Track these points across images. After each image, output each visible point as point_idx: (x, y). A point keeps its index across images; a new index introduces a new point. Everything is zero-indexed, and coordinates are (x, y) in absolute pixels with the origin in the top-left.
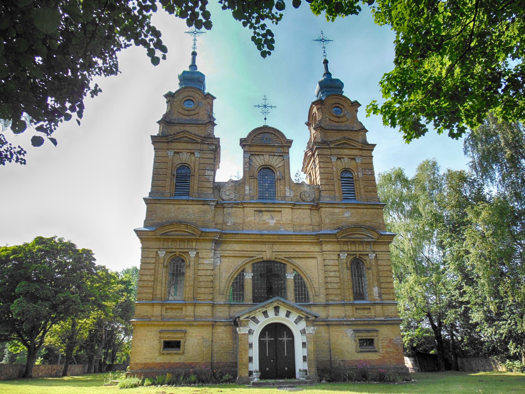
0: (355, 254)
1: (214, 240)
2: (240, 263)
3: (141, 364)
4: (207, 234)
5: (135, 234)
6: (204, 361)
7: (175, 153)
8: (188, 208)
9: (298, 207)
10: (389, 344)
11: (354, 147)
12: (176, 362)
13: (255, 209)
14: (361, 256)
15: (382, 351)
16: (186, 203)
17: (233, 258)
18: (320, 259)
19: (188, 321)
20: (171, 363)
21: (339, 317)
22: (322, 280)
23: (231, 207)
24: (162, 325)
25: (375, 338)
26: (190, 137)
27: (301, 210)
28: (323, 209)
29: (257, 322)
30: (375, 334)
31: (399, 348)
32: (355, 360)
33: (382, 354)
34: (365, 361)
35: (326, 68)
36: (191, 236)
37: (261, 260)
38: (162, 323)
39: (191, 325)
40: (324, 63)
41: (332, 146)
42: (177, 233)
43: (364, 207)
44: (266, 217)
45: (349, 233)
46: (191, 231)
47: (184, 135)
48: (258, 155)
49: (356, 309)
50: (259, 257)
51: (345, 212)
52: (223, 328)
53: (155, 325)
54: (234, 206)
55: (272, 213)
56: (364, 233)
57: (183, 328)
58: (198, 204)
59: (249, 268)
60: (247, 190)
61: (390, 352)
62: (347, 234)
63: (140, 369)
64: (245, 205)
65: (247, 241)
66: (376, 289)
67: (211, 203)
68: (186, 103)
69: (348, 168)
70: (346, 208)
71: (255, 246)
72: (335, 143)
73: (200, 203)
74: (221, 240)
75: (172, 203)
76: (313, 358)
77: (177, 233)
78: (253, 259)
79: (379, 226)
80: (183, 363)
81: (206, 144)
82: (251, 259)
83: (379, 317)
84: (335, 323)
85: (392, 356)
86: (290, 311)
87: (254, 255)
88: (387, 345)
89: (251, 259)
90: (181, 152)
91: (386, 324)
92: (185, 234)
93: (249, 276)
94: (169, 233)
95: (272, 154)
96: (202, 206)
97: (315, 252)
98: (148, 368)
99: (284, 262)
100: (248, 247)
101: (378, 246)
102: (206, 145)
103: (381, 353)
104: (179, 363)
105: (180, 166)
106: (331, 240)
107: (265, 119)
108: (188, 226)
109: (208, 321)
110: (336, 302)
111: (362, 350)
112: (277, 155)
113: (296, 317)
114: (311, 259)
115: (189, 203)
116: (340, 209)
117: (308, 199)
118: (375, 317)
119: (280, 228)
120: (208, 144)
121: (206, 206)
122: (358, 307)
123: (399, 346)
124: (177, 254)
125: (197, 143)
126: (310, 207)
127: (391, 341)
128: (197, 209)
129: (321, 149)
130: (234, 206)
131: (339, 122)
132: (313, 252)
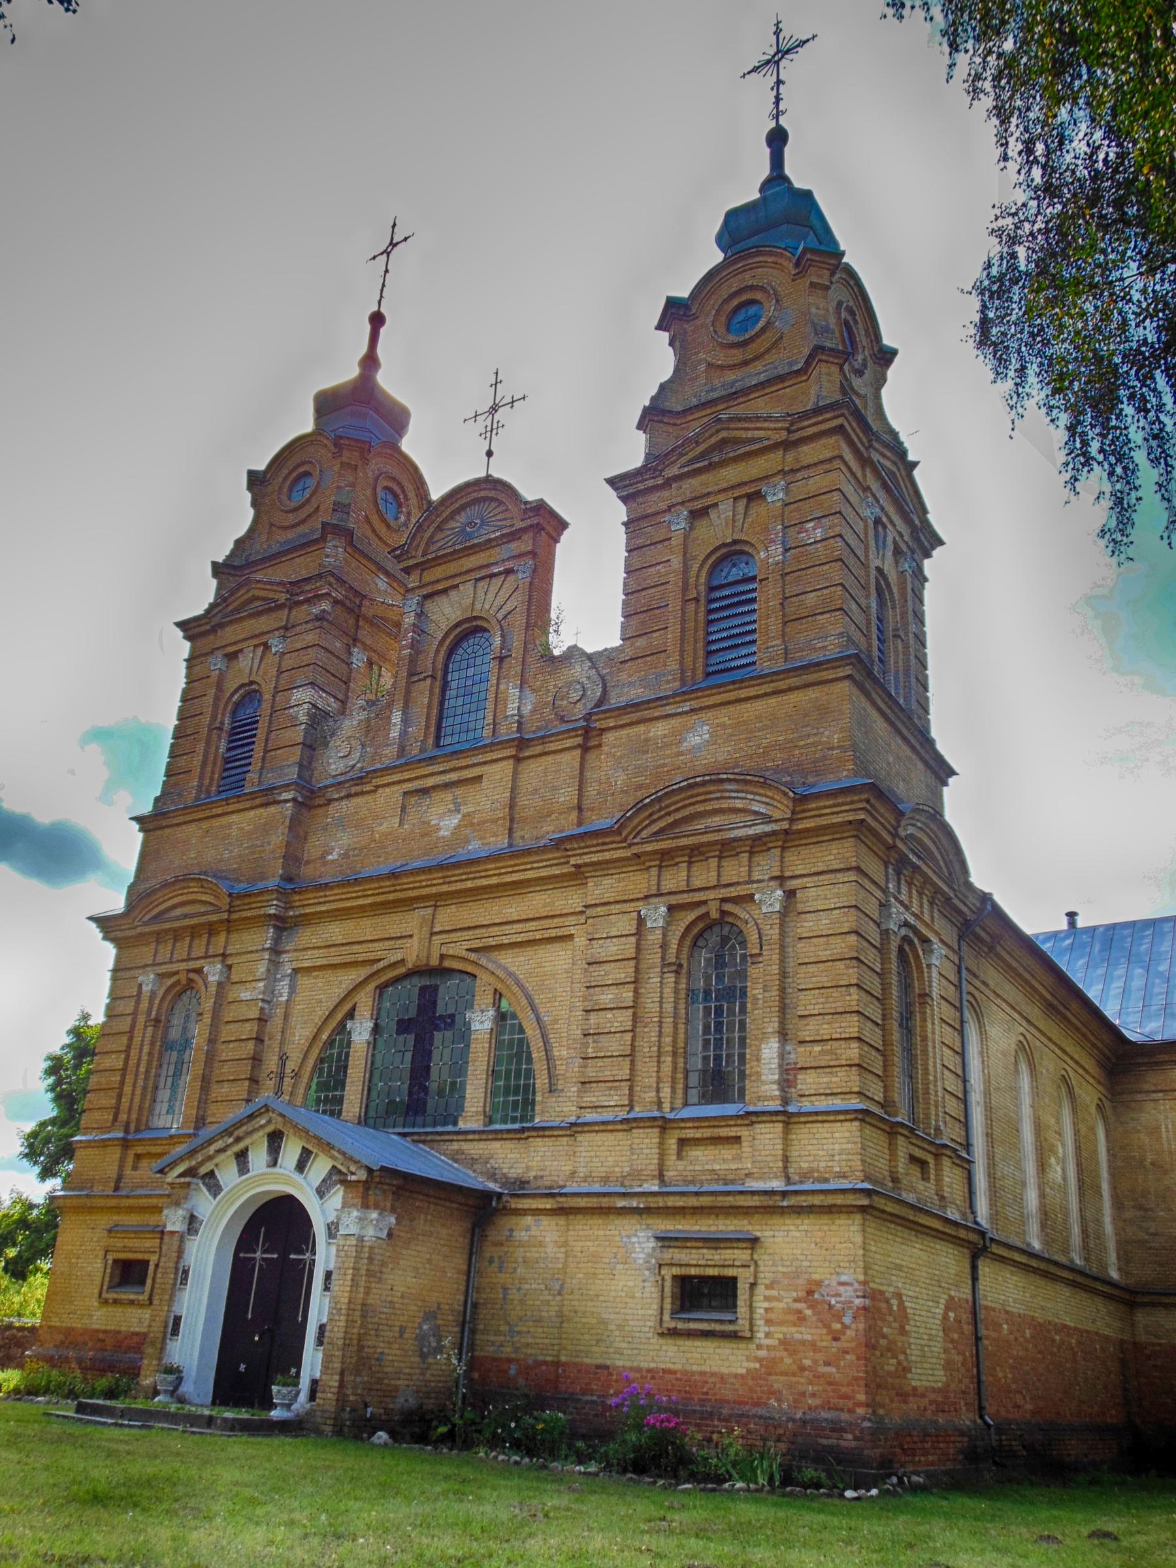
0: (705, 902)
4: (247, 900)
5: (95, 931)
7: (227, 656)
8: (230, 825)
9: (538, 749)
11: (757, 446)
12: (132, 1329)
13: (408, 786)
14: (728, 907)
15: (767, 1335)
20: (119, 1332)
21: (605, 1180)
24: (117, 1209)
25: (744, 1277)
27: (550, 758)
28: (609, 737)
29: (215, 1189)
30: (742, 1255)
31: (845, 1327)
32: (649, 1371)
33: (762, 1353)
34: (687, 1378)
35: (777, 161)
38: (113, 1202)
45: (678, 816)
50: (393, 959)
53: (101, 1209)
55: (458, 791)
56: (739, 804)
58: (252, 808)
59: (365, 1002)
60: (395, 725)
61: (803, 1343)
62: (670, 819)
69: (735, 542)
71: (386, 919)
72: (682, 455)
73: (258, 801)
74: (291, 913)
76: (341, 1335)
78: (376, 967)
79: (824, 758)
82: (368, 970)
83: (762, 1177)
85: (807, 1362)
86: (310, 1148)
87: (372, 956)
88: (789, 1311)
89: (368, 970)
91: (798, 1211)
92: (203, 909)
95: (483, 573)
96: (261, 810)
97: (566, 915)
100: (366, 928)
101: (804, 851)
103: (759, 1347)
105: (243, 697)
106: (607, 856)
107: (489, 454)
110: (607, 1116)
111: (680, 1325)
112: (500, 574)
113: (233, 1167)
114: (556, 946)
116: (674, 722)
120: (307, 601)
121: (273, 809)
122: (690, 1134)
123: (847, 1320)
127: (810, 1293)
129: (640, 500)
132: (561, 915)
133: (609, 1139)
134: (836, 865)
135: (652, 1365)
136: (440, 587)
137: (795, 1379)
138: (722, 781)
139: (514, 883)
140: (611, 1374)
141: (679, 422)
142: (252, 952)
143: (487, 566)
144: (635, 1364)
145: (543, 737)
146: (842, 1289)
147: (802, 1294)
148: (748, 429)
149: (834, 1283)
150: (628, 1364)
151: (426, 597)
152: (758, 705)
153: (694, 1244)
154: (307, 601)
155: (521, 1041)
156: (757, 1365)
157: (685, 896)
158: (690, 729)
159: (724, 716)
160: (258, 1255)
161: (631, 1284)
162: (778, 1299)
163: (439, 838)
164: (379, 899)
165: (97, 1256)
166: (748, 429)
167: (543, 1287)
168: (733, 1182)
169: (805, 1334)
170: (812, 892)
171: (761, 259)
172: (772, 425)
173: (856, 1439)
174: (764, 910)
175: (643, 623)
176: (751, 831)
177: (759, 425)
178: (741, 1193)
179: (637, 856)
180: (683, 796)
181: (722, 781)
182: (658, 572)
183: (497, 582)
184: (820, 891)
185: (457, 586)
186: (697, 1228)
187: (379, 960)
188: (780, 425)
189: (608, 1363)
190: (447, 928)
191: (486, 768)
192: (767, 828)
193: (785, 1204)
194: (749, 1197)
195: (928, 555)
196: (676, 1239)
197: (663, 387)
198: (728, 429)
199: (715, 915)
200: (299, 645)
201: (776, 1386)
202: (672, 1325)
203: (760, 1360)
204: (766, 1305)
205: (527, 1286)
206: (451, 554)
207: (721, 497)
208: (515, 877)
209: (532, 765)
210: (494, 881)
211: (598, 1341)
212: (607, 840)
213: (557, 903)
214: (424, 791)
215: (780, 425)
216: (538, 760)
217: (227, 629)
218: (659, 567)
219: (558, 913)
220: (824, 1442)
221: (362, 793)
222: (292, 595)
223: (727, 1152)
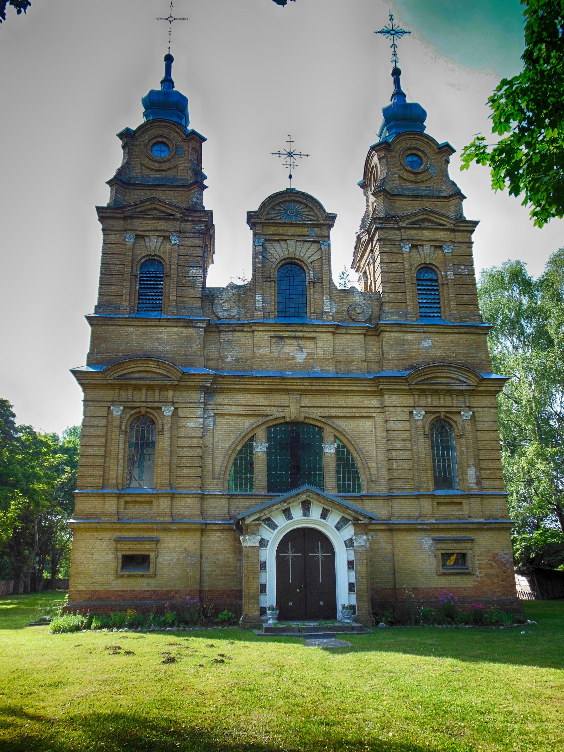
0: (439, 412)
1: (204, 387)
2: (247, 425)
3: (86, 592)
4: (192, 377)
8: (160, 333)
9: (344, 331)
10: (491, 562)
11: (441, 227)
12: (143, 589)
13: (272, 334)
15: (480, 573)
19: (161, 523)
20: (135, 591)
22: (382, 456)
23: (232, 331)
24: (120, 530)
25: (469, 552)
26: (162, 208)
27: (349, 336)
28: (387, 335)
30: (469, 545)
31: (507, 568)
32: (435, 588)
33: (479, 579)
37: (282, 421)
38: (118, 526)
40: (393, 75)
41: (404, 224)
43: (455, 331)
44: (290, 348)
45: (429, 376)
46: (165, 373)
48: (278, 241)
50: (278, 416)
51: (422, 340)
52: (219, 534)
53: (106, 530)
56: (454, 376)
57: (154, 535)
58: (176, 327)
59: (261, 434)
60: (258, 301)
61: (493, 575)
62: (426, 377)
63: (84, 600)
64: (253, 328)
66: (472, 471)
67: (199, 325)
71: (271, 396)
72: (408, 219)
73: (181, 324)
74: (215, 386)
78: (268, 418)
80: (155, 592)
81: (189, 221)
82: (265, 419)
83: (476, 517)
87: (269, 413)
89: (265, 419)
90: (147, 236)
95: (301, 238)
97: (371, 407)
98: (98, 598)
99: (319, 424)
101: (477, 398)
104: (148, 591)
106: (398, 387)
107: (290, 177)
108: (160, 364)
110: (405, 493)
111: (446, 571)
112: (310, 241)
114: (364, 420)
115: (161, 324)
118: (470, 517)
119: (313, 367)
121: (190, 330)
122: (442, 501)
125: (175, 219)
127: (494, 557)
128: (175, 334)
129: (385, 231)
132: (368, 407)
133: (408, 502)
134: (489, 405)
135: (436, 586)
136: (276, 238)
137: (492, 587)
138: (450, 366)
139: (346, 390)
140: (419, 591)
141: (391, 198)
142: (192, 403)
143: (304, 236)
144: (429, 586)
145: (347, 326)
146: (505, 556)
147: (491, 558)
148: (437, 218)
149: (502, 554)
150: (426, 586)
151: (266, 240)
152: (451, 336)
153: (450, 542)
154: (193, 221)
155: (348, 458)
156: (477, 583)
157: (431, 408)
158: (424, 340)
159: (436, 337)
160: (320, 554)
161: (424, 557)
162: (483, 560)
163: (296, 362)
164: (271, 387)
165: (207, 558)
166: (437, 218)
167: (382, 559)
168: (462, 519)
169: (494, 571)
170: (481, 414)
171: (421, 138)
172: (448, 220)
173: (517, 605)
174: (464, 418)
175: (393, 287)
176: (461, 388)
177: (443, 218)
178: (469, 523)
179: (410, 389)
180: (433, 369)
181: (450, 366)
182: (397, 267)
183: (308, 245)
184: (484, 414)
185: (286, 240)
186: (449, 536)
187: (268, 416)
188: (452, 222)
189: (417, 587)
190: (308, 405)
191: (317, 334)
192: (468, 388)
193: (486, 527)
194: (472, 525)
195: (204, 207)
196: (443, 540)
198: (428, 215)
199: (442, 417)
200: (190, 244)
201: (485, 590)
202: (444, 571)
203: (478, 581)
204: (479, 562)
205: (374, 560)
206: (283, 223)
207: (424, 243)
208: (347, 388)
209: (341, 337)
210: (336, 388)
211: (412, 579)
212: (400, 381)
213: (365, 402)
214: (281, 338)
215: (452, 222)
216: (343, 335)
217: (135, 221)
218: (397, 264)
219: (366, 406)
220: (507, 607)
221: (243, 331)
222: (184, 216)
223: (455, 508)
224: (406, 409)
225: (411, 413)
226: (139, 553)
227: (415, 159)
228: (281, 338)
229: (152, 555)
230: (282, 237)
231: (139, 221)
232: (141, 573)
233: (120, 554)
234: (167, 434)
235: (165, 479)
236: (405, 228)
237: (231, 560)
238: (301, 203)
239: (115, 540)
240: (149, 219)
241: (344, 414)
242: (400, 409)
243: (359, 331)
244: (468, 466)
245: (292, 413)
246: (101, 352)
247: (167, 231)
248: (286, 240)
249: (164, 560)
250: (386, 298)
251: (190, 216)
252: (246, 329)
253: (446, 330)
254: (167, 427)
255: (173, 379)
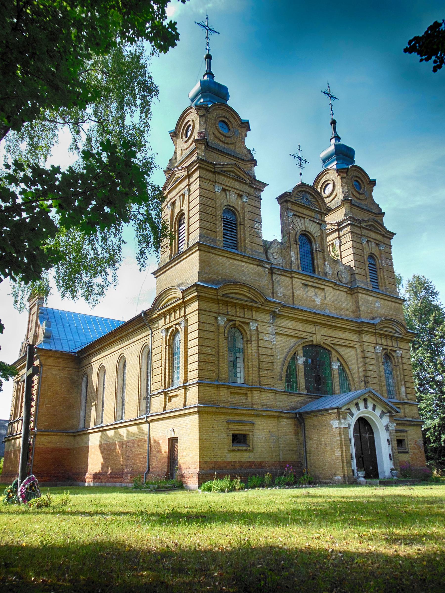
0: (235, 321)
1: (274, 312)
2: (292, 344)
3: (211, 463)
4: (269, 304)
6: (273, 460)
12: (247, 460)
13: (303, 282)
16: (242, 259)
17: (286, 337)
18: (359, 350)
19: (257, 410)
22: (362, 374)
23: (280, 274)
24: (229, 414)
26: (238, 173)
28: (360, 295)
30: (405, 435)
36: (250, 302)
37: (310, 343)
39: (258, 416)
40: (331, 124)
41: (363, 225)
42: (238, 296)
43: (390, 299)
44: (311, 292)
46: (253, 298)
47: (232, 169)
48: (299, 217)
49: (231, 393)
51: (376, 302)
52: (285, 420)
53: (222, 413)
54: (283, 273)
55: (317, 290)
56: (394, 328)
57: (250, 419)
63: (210, 469)
64: (293, 275)
65: (300, 319)
66: (403, 388)
67: (266, 266)
68: (221, 124)
70: (377, 297)
73: (256, 263)
75: (226, 255)
77: (238, 296)
80: (253, 462)
81: (252, 187)
84: (407, 423)
87: (305, 337)
90: (228, 190)
91: (414, 425)
92: (245, 299)
93: (301, 361)
94: (229, 295)
95: (312, 219)
96: (255, 267)
98: (219, 467)
99: (329, 349)
102: (252, 189)
104: (249, 462)
107: (301, 174)
108: (251, 290)
109: (276, 412)
114: (350, 349)
115: (244, 260)
117: (344, 280)
118: (405, 417)
119: (325, 309)
120: (255, 188)
121: (260, 268)
124: (237, 323)
125: (246, 184)
126: (346, 290)
128: (252, 269)
130: (283, 273)
131: (359, 199)
136: (299, 215)
154: (255, 188)
159: (382, 302)
160: (368, 435)
164: (308, 319)
197: (378, 205)
214: (306, 285)
217: (221, 177)
224: (373, 345)
225: (216, 318)
226: (240, 432)
227: (357, 184)
228: (306, 285)
229: (251, 433)
230: (302, 215)
231: (223, 178)
232: (245, 448)
233: (231, 433)
234: (254, 344)
235: (255, 377)
236: (364, 228)
237: (294, 439)
238: (311, 194)
239: (227, 422)
240: (229, 178)
241: (342, 344)
242: (370, 344)
243: (345, 290)
244: (402, 385)
245: (318, 339)
246: (207, 273)
247: (241, 191)
248: (304, 218)
249: (257, 438)
250: (357, 271)
251: (254, 184)
252: (288, 275)
253: (387, 298)
254: (254, 338)
255: (258, 304)
